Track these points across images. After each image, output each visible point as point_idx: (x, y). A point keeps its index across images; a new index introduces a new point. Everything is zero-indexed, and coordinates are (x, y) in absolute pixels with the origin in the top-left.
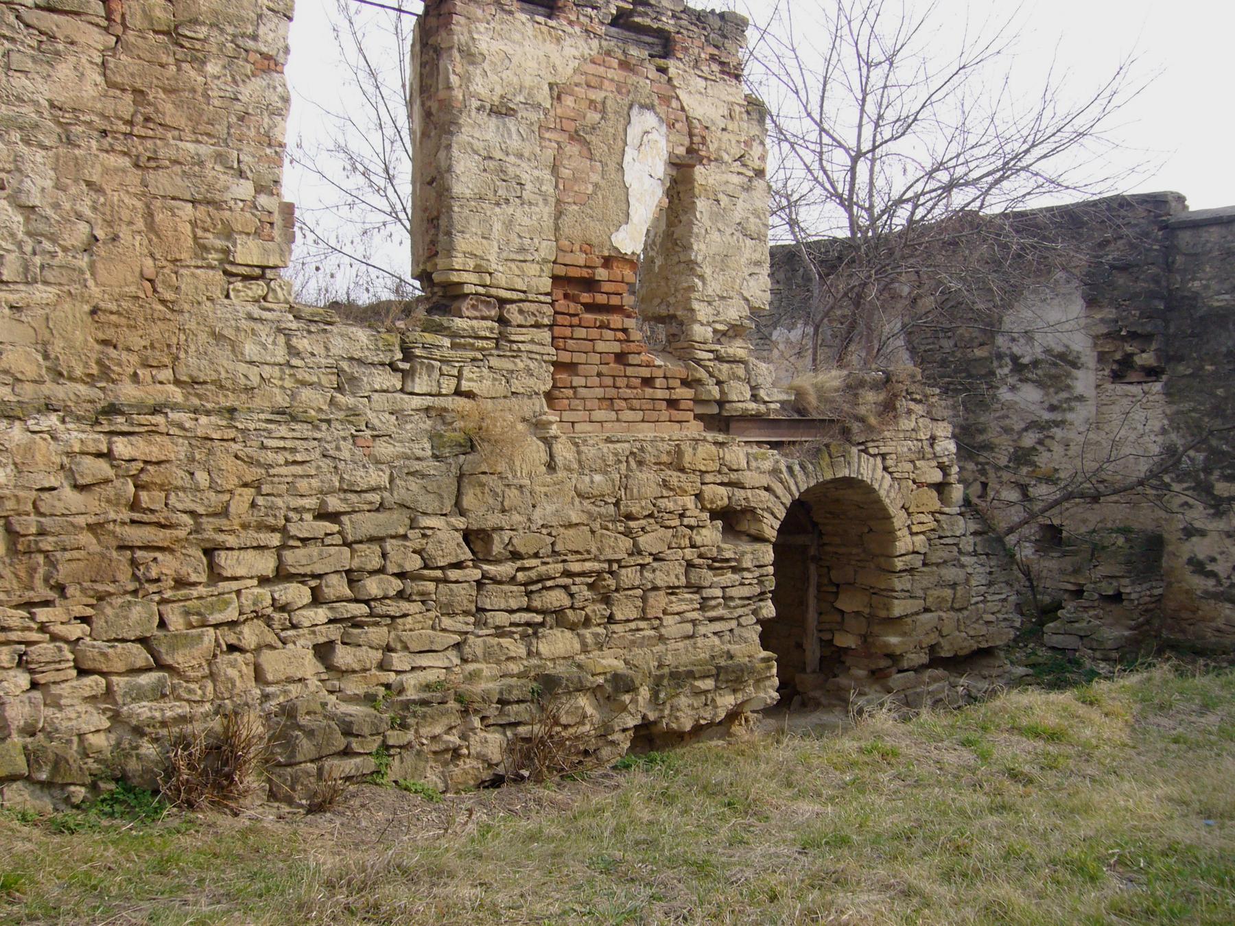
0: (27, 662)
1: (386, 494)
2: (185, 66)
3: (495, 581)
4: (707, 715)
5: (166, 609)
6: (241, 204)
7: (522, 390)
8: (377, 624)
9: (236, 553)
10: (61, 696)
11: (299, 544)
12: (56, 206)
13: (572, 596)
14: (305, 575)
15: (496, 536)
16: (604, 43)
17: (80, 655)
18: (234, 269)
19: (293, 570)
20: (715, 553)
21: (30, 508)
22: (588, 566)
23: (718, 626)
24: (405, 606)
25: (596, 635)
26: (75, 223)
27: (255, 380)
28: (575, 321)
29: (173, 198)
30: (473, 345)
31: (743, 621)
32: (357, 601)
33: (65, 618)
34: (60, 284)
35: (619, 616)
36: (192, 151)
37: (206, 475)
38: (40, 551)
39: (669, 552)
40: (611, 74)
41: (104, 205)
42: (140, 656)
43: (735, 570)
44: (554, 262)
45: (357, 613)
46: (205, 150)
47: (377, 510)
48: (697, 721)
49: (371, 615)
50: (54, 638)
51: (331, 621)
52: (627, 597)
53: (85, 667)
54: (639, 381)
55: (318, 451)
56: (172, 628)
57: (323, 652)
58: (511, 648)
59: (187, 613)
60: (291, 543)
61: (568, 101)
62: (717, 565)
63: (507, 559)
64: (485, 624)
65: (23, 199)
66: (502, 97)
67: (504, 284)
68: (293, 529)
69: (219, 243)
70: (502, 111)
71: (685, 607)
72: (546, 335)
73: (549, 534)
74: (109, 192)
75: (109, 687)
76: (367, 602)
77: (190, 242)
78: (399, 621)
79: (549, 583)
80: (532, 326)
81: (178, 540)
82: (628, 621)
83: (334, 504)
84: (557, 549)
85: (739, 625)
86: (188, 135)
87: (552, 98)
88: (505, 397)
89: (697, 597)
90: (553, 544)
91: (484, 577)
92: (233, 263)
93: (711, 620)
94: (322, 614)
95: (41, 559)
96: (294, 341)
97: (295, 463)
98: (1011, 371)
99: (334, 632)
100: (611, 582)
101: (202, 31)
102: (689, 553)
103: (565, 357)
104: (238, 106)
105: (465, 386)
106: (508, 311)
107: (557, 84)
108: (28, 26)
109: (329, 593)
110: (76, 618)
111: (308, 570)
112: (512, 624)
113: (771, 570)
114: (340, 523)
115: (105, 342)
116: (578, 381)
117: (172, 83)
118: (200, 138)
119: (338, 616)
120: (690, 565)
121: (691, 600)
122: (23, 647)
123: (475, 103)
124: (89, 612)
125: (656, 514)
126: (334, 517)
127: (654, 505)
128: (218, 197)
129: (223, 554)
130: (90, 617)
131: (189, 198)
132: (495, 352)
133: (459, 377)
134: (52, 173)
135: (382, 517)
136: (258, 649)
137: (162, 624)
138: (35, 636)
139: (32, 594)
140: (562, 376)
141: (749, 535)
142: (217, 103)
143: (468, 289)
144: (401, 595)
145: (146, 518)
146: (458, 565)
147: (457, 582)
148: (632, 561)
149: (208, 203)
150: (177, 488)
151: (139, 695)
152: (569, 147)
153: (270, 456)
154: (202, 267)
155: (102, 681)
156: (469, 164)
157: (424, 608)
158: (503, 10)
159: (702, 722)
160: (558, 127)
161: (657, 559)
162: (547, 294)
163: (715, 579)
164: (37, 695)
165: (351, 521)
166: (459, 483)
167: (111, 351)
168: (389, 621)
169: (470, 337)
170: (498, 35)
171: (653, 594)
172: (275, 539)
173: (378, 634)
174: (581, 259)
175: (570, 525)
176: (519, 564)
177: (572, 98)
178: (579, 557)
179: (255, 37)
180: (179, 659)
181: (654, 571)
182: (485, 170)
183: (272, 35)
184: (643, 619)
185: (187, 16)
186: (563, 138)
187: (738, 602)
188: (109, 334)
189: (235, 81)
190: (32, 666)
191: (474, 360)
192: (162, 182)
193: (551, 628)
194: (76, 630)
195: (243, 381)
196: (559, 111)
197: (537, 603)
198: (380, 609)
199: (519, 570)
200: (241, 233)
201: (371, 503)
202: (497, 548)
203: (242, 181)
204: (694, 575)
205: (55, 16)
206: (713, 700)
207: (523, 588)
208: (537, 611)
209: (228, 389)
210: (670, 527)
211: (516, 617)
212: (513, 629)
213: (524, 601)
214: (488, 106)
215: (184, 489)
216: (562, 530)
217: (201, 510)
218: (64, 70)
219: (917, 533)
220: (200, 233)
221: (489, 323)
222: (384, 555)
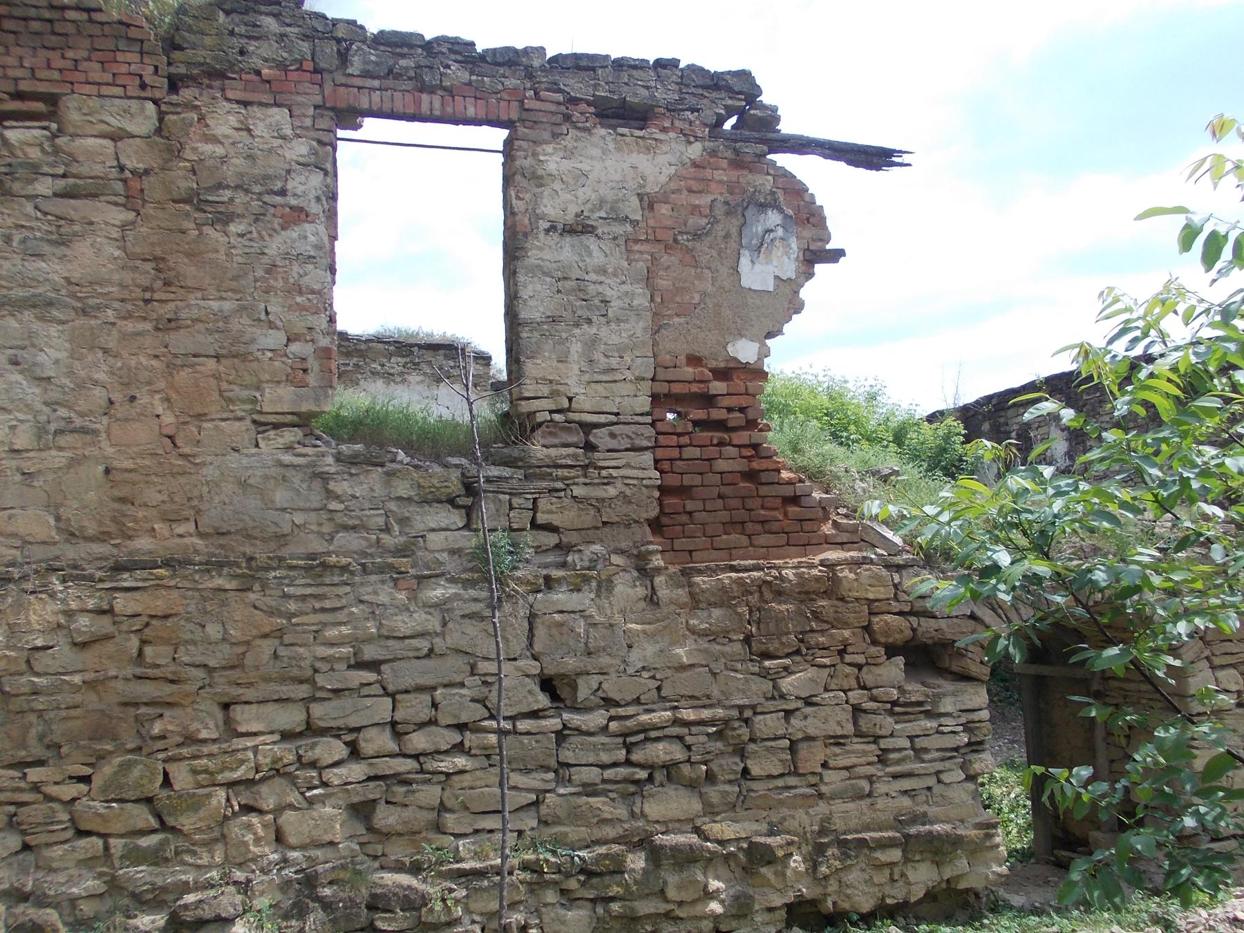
0: (19, 824)
1: (437, 640)
2: (208, 230)
3: (580, 731)
4: (896, 895)
5: (171, 768)
6: (269, 354)
7: (617, 519)
8: (428, 781)
9: (254, 707)
10: (52, 859)
11: (330, 695)
12: (71, 373)
13: (689, 748)
14: (339, 729)
15: (581, 682)
16: (707, 144)
17: (76, 815)
18: (262, 419)
19: (322, 724)
20: (895, 693)
21: (24, 667)
22: (706, 714)
23: (906, 784)
24: (461, 761)
25: (725, 794)
26: (89, 389)
27: (286, 529)
28: (685, 440)
29: (195, 356)
30: (551, 474)
31: (946, 778)
32: (406, 756)
33: (58, 778)
34: (75, 448)
35: (755, 770)
36: (216, 309)
37: (219, 627)
38: (33, 711)
39: (826, 695)
40: (720, 176)
41: (120, 369)
42: (142, 817)
43: (929, 715)
44: (653, 380)
45: (401, 769)
46: (228, 306)
47: (428, 656)
48: (883, 899)
49: (422, 771)
50: (49, 798)
51: (370, 779)
52: (768, 749)
53: (82, 828)
54: (779, 501)
55: (352, 596)
56: (176, 787)
57: (362, 811)
58: (606, 808)
59: (195, 772)
60: (319, 694)
61: (664, 209)
62: (897, 709)
63: (599, 707)
64: (570, 780)
65: (38, 373)
66: (577, 215)
67: (588, 407)
68: (320, 680)
69: (245, 394)
70: (578, 229)
71: (854, 760)
72: (647, 458)
73: (653, 677)
74: (125, 355)
75: (107, 848)
76: (416, 757)
77: (216, 395)
78: (456, 778)
79: (653, 734)
80: (627, 450)
81: (187, 695)
82: (770, 777)
83: (370, 653)
84: (663, 693)
85: (939, 781)
86: (213, 292)
87: (643, 209)
88: (597, 528)
89: (873, 747)
90: (659, 689)
91: (565, 726)
92: (261, 413)
93: (896, 776)
94: (356, 771)
95: (33, 718)
96: (332, 485)
97: (323, 610)
98: (209, 852)
99: (374, 791)
100: (744, 732)
101: (226, 195)
102: (856, 696)
103: (673, 480)
104: (265, 260)
105: (541, 518)
106: (595, 435)
107: (648, 194)
108: (46, 214)
109: (367, 748)
110: (71, 778)
111: (340, 723)
112: (604, 781)
113: (985, 714)
114: (379, 672)
115: (122, 500)
116: (690, 505)
117: (193, 246)
118: (224, 294)
119: (380, 773)
120: (857, 710)
121: (865, 753)
122: (12, 809)
123: (544, 225)
124: (87, 771)
125: (804, 651)
126: (374, 666)
127: (801, 641)
128: (242, 349)
129: (238, 708)
130: (90, 776)
131: (213, 353)
132: (582, 480)
133: (535, 509)
134: (67, 345)
135: (430, 663)
136: (279, 810)
137: (167, 782)
138: (26, 797)
139: (23, 753)
140: (671, 501)
141: (951, 673)
142: (240, 260)
143: (540, 417)
144: (459, 748)
145: (151, 672)
146: (535, 714)
147: (528, 733)
148: (770, 705)
149: (234, 356)
150: (187, 642)
151: (136, 856)
152: (666, 257)
153: (292, 606)
154: (228, 419)
155: (99, 843)
156: (538, 287)
157: (486, 764)
158: (577, 128)
159: (889, 901)
160: (651, 237)
161: (808, 702)
162: (647, 414)
163: (898, 727)
164: (29, 857)
165: (393, 670)
166: (530, 623)
167: (126, 508)
168: (443, 778)
169: (548, 466)
170: (569, 154)
171: (805, 745)
172: (303, 691)
173: (430, 794)
174: (689, 372)
175: (683, 668)
176: (613, 712)
177: (668, 206)
178: (696, 703)
179: (283, 192)
180: (187, 822)
181: (806, 717)
182: (559, 291)
183: (302, 188)
184: (796, 773)
185: (210, 183)
186: (656, 249)
187: (936, 755)
188: (124, 491)
189: (262, 238)
190: (24, 827)
191: (552, 491)
192: (181, 341)
193: (662, 785)
194: (69, 791)
195: (273, 529)
196: (651, 222)
197: (636, 756)
198: (431, 765)
199: (611, 719)
200: (268, 382)
201: (418, 650)
202: (583, 692)
203: (271, 331)
204: (865, 723)
205: (72, 201)
206: (903, 875)
207: (620, 740)
208: (642, 766)
209: (256, 538)
210: (825, 666)
211: (609, 774)
212: (609, 787)
213: (621, 754)
214: (560, 226)
215: (194, 643)
216: (669, 673)
217: (212, 663)
218: (82, 248)
219: (1223, 667)
220: (224, 386)
221: (571, 450)
222: (435, 705)
